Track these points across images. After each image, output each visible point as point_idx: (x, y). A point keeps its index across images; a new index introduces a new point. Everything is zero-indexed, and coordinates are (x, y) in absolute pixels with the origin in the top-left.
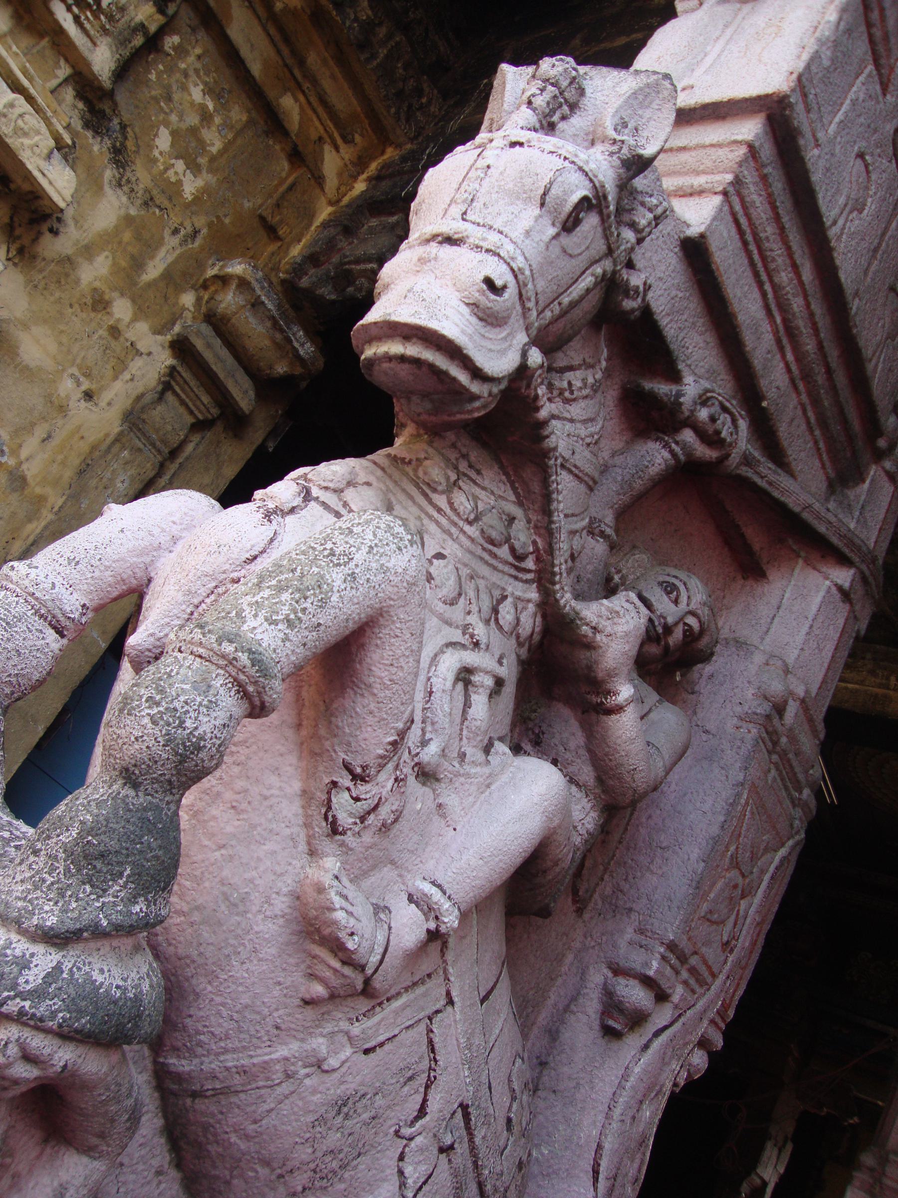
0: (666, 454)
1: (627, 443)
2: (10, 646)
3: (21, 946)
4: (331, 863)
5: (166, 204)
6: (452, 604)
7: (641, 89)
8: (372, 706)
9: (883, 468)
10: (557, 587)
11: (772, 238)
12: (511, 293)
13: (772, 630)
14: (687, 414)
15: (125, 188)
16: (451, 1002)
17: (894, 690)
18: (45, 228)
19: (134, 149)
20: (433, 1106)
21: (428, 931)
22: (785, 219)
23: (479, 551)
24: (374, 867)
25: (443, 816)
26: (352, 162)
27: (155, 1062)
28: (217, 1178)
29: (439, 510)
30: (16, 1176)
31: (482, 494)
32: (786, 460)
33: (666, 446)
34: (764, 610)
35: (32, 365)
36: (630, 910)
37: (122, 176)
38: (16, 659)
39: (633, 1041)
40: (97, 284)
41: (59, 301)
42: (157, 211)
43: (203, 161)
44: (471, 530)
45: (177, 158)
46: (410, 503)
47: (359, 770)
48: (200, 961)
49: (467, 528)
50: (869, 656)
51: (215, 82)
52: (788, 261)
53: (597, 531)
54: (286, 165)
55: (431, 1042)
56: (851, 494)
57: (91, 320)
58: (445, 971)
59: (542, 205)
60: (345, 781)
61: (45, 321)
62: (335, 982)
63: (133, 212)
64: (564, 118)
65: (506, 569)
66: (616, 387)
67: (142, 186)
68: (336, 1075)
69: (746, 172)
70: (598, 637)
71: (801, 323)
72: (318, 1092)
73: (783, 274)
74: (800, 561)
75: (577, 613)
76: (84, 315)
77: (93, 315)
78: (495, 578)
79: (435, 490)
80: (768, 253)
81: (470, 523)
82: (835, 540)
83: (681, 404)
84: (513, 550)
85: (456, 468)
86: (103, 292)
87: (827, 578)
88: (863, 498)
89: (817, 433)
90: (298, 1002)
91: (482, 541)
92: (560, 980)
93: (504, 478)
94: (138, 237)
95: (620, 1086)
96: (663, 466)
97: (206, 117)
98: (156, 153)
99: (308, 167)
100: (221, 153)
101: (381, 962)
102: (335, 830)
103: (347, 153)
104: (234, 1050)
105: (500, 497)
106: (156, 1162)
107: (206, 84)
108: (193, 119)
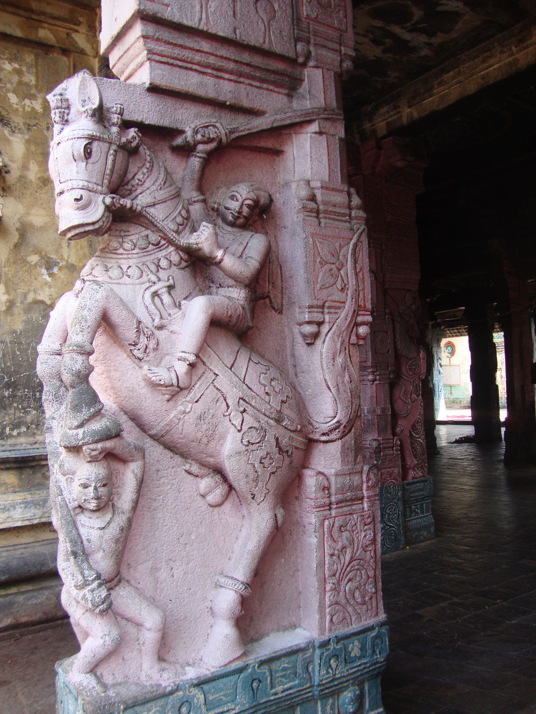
0: (197, 159)
1: (186, 162)
2: (50, 367)
3: (75, 432)
4: (146, 367)
5: (35, 121)
6: (141, 277)
7: (80, 85)
8: (123, 328)
9: (310, 67)
10: (177, 241)
11: (180, 53)
12: (84, 193)
13: (296, 170)
14: (193, 142)
15: (17, 131)
16: (217, 375)
17: (517, 53)
18: (4, 174)
19: (6, 113)
20: (230, 404)
21: (188, 365)
22: (180, 42)
23: (142, 254)
24: (162, 359)
25: (175, 333)
26: (88, 31)
27: (148, 435)
28: (186, 451)
29: (122, 254)
30: (123, 473)
31: (131, 237)
32: (256, 110)
33: (196, 156)
34: (290, 164)
35: (42, 224)
36: (294, 302)
37: (11, 128)
38: (54, 369)
39: (319, 342)
40: (38, 176)
41: (31, 194)
42: (35, 128)
43: (33, 91)
44: (136, 251)
45: (23, 100)
46: (112, 260)
47: (133, 343)
48: (136, 408)
49: (133, 252)
50: (496, 44)
51: (10, 54)
52: (194, 52)
53: (192, 202)
54: (65, 59)
55: (217, 389)
56: (301, 90)
57: (48, 190)
58: (209, 369)
59: (75, 161)
60: (133, 348)
61: (33, 206)
62: (169, 392)
63: (27, 137)
64: (68, 114)
65: (155, 251)
66: (168, 150)
67: (21, 124)
68: (192, 412)
69: (149, 45)
70: (199, 245)
71: (220, 64)
72: (190, 419)
73: (196, 57)
74: (294, 135)
75: (189, 243)
76: (44, 191)
77: (46, 188)
78: (153, 257)
79: (117, 250)
80: (183, 58)
81: (134, 249)
82: (298, 120)
83: (188, 142)
84: (153, 244)
85: (121, 236)
86: (43, 177)
87: (308, 133)
88: (307, 87)
89: (265, 86)
90: (166, 402)
91: (141, 251)
92: (287, 337)
93: (137, 226)
94: (37, 144)
95: (322, 358)
96: (199, 164)
97: (19, 72)
98: (15, 106)
99: (73, 51)
100: (37, 81)
101: (178, 380)
102: (140, 360)
103: (83, 29)
104: (161, 422)
105: (140, 232)
106: (169, 456)
107: (7, 59)
108: (15, 79)
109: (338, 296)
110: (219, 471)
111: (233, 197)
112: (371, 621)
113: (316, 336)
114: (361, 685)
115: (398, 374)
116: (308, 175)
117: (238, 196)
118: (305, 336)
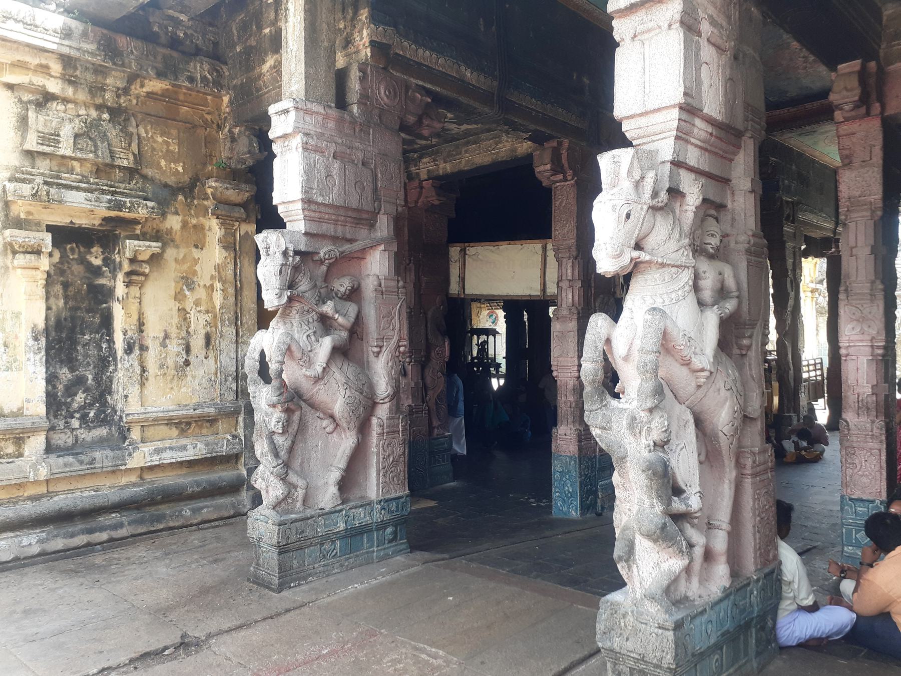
34: (369, 266)
39: (380, 356)
109: (391, 333)
110: (332, 417)
111: (341, 285)
112: (401, 494)
113: (379, 353)
114: (396, 526)
115: (428, 358)
116: (378, 272)
117: (343, 285)
118: (374, 353)
